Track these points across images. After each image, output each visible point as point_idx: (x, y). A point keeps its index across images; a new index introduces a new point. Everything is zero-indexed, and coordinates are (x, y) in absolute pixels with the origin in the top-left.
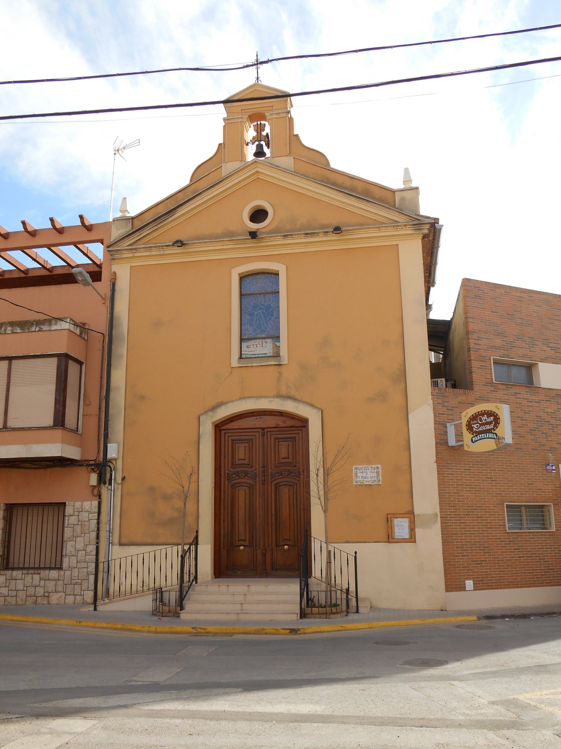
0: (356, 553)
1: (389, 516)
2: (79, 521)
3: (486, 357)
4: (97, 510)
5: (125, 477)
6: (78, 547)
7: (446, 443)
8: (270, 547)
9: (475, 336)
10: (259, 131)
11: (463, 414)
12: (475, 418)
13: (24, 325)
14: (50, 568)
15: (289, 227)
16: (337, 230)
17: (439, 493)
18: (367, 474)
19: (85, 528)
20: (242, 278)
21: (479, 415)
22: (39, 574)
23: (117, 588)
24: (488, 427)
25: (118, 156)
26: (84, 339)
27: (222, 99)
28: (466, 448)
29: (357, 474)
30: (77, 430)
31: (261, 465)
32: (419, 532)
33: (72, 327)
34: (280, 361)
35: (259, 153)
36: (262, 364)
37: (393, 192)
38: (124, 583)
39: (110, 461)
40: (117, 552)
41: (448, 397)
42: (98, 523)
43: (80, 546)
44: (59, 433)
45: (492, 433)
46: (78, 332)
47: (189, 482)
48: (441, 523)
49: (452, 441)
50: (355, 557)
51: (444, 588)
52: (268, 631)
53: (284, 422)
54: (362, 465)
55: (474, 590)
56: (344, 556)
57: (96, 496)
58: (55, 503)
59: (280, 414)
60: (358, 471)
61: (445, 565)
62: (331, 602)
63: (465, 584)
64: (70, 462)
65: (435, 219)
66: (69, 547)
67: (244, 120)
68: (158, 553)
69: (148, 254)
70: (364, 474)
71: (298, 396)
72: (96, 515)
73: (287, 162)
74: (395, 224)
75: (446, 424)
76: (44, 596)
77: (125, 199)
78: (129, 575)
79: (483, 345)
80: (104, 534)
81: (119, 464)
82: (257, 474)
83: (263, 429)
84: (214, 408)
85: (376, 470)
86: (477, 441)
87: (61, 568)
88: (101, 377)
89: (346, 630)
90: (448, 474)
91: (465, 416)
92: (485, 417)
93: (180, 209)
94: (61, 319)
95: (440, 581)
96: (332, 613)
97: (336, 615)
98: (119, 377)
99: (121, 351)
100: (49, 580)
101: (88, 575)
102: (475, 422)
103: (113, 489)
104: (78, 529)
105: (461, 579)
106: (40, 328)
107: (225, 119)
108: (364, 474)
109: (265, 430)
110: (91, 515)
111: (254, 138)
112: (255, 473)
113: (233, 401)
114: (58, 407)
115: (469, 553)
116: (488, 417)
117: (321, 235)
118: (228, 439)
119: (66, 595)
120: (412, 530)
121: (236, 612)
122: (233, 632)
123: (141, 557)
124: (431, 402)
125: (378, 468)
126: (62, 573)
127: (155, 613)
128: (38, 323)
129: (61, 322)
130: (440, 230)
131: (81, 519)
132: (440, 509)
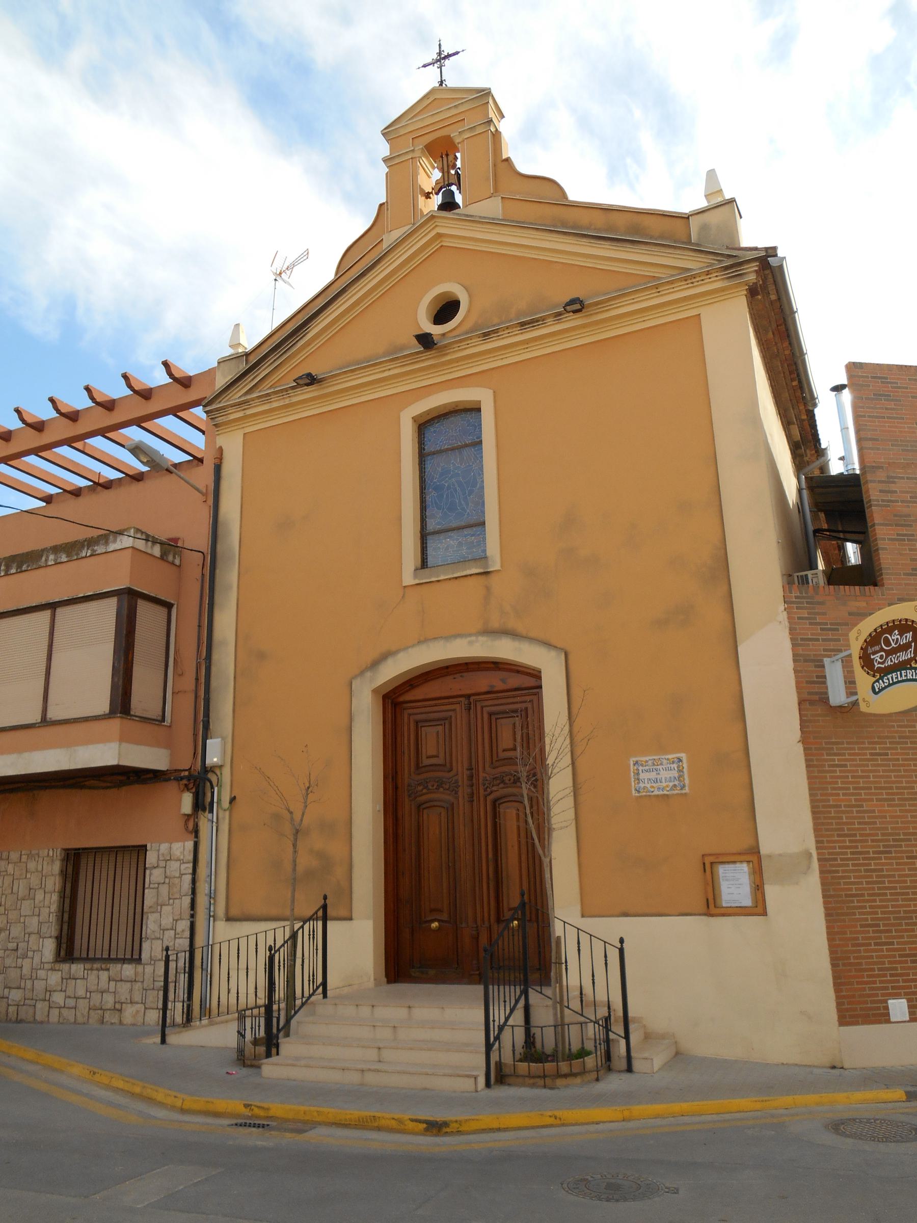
0: (622, 941)
1: (708, 861)
2: (166, 877)
3: (909, 516)
4: (191, 857)
5: (235, 798)
6: (163, 923)
7: (824, 699)
8: (487, 924)
9: (881, 475)
11: (853, 634)
12: (874, 639)
13: (71, 549)
14: (124, 961)
16: (576, 306)
17: (813, 807)
18: (659, 774)
19: (175, 890)
20: (423, 426)
21: (884, 631)
22: (108, 970)
24: (903, 656)
25: (280, 283)
26: (173, 564)
27: (430, 61)
28: (863, 708)
29: (638, 774)
30: (163, 720)
31: (466, 766)
32: (771, 891)
33: (141, 545)
34: (487, 566)
35: (449, 205)
36: (455, 575)
37: (685, 218)
39: (212, 769)
40: (223, 931)
41: (822, 603)
42: (194, 881)
43: (167, 921)
44: (116, 724)
45: (911, 668)
46: (157, 551)
47: (305, 802)
48: (821, 872)
49: (838, 695)
51: (836, 1017)
52: (383, 1122)
53: (503, 681)
54: (646, 756)
57: (191, 832)
58: (134, 846)
59: (495, 665)
60: (641, 768)
61: (834, 965)
62: (570, 1049)
63: (887, 1008)
64: (151, 775)
65: (767, 249)
66: (151, 924)
67: (417, 154)
69: (266, 407)
70: (653, 775)
71: (520, 628)
72: (191, 865)
73: (492, 207)
74: (688, 277)
75: (822, 661)
76: (115, 1009)
77: (237, 325)
79: (901, 492)
80: (202, 901)
82: (460, 783)
83: (468, 696)
84: (375, 664)
86: (883, 689)
87: (139, 960)
88: (199, 626)
89: (563, 1125)
91: (857, 639)
92: (896, 635)
94: (120, 533)
95: (823, 998)
96: (559, 1075)
97: (570, 1080)
98: (225, 623)
100: (121, 980)
102: (877, 648)
103: (215, 820)
104: (164, 890)
105: (877, 995)
106: (94, 551)
107: (385, 160)
109: (472, 698)
110: (183, 866)
111: (437, 182)
112: (457, 782)
113: (406, 648)
114: (116, 680)
115: (894, 937)
116: (901, 635)
117: (550, 321)
118: (409, 719)
119: (146, 1008)
120: (758, 889)
121: (359, 1067)
122: (318, 1119)
123: (234, 944)
124: (783, 616)
126: (140, 968)
128: (91, 542)
129: (121, 537)
130: (781, 267)
132: (817, 842)
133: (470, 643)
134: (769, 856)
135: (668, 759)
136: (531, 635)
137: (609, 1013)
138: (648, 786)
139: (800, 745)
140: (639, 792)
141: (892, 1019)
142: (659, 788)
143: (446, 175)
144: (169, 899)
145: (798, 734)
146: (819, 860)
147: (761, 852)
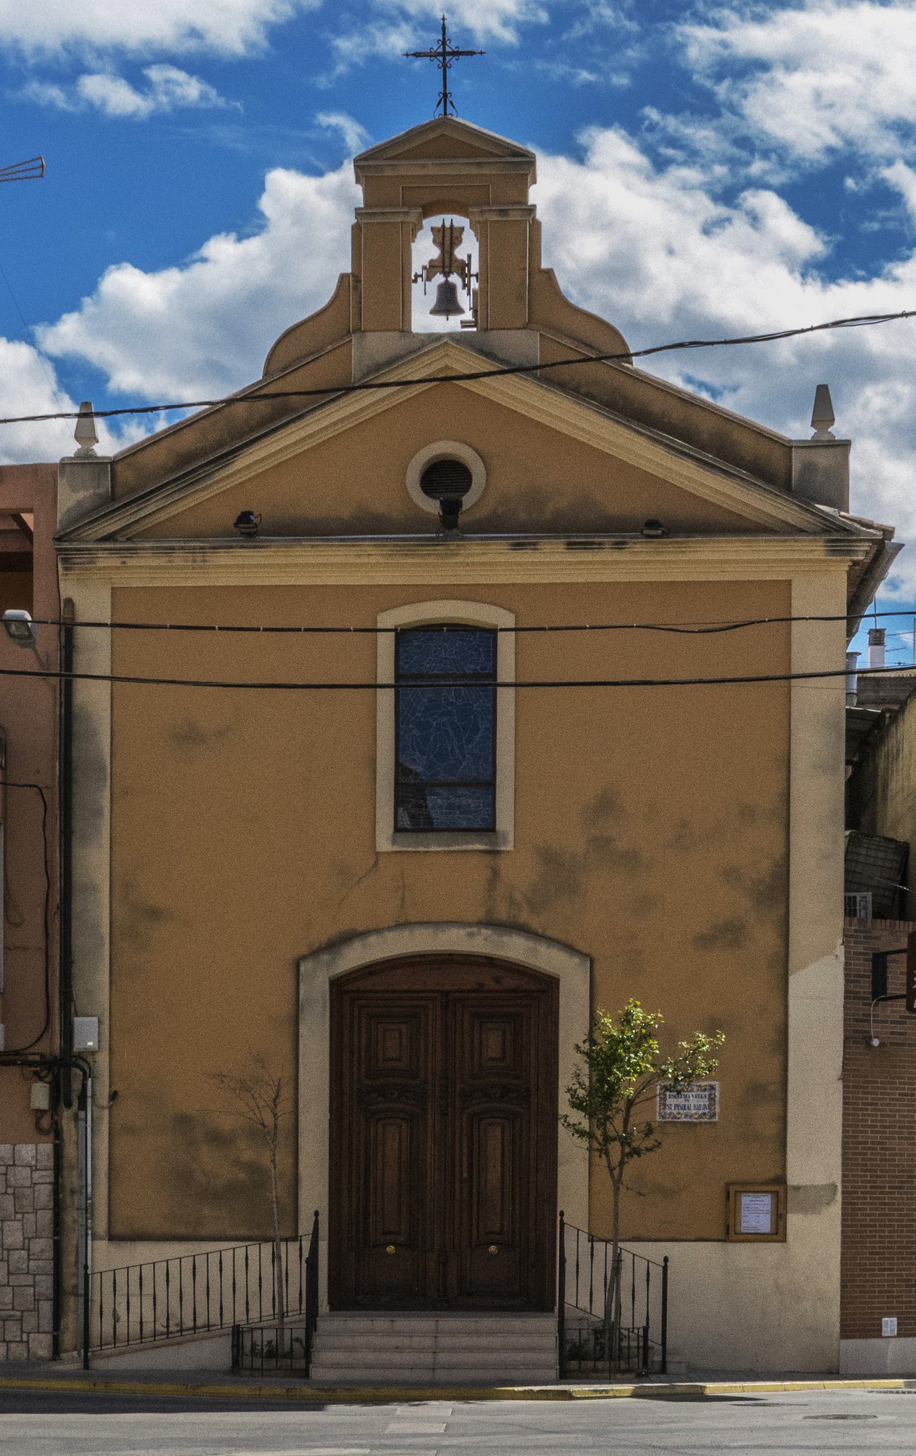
0: (666, 1260)
1: (732, 1189)
2: (7, 1186)
4: (50, 1163)
10: (447, 246)
15: (523, 516)
19: (25, 1202)
23: (108, 1327)
29: (665, 1099)
32: (794, 1221)
38: (124, 1318)
39: (81, 1056)
48: (843, 1203)
50: (665, 1269)
53: (497, 980)
55: (899, 1335)
56: (641, 1267)
59: (491, 962)
68: (227, 1257)
71: (535, 923)
72: (50, 1173)
78: (135, 1301)
81: (102, 1061)
82: (430, 1093)
83: (447, 993)
84: (336, 944)
85: (707, 1093)
90: (866, 1104)
93: (247, 451)
98: (95, 862)
99: (98, 799)
101: (37, 1300)
107: (358, 212)
108: (681, 1101)
110: (36, 1175)
113: (378, 931)
124: (840, 951)
125: (712, 1088)
127: (236, 1367)
131: (12, 1181)
133: (471, 935)
134: (797, 1188)
135: (700, 1086)
136: (549, 933)
137: (648, 1323)
138: (675, 1112)
139: (841, 1082)
140: (663, 1117)
141: (883, 1334)
142: (686, 1116)
143: (447, 256)
144: (16, 1213)
145: (839, 1072)
146: (843, 1192)
147: (789, 1183)
